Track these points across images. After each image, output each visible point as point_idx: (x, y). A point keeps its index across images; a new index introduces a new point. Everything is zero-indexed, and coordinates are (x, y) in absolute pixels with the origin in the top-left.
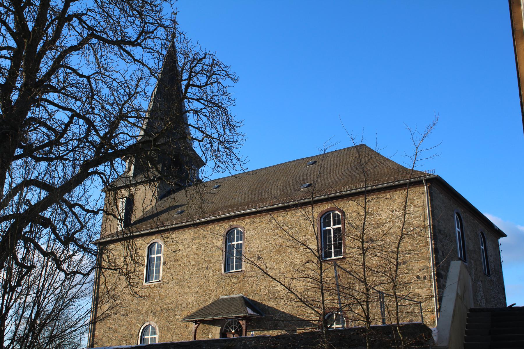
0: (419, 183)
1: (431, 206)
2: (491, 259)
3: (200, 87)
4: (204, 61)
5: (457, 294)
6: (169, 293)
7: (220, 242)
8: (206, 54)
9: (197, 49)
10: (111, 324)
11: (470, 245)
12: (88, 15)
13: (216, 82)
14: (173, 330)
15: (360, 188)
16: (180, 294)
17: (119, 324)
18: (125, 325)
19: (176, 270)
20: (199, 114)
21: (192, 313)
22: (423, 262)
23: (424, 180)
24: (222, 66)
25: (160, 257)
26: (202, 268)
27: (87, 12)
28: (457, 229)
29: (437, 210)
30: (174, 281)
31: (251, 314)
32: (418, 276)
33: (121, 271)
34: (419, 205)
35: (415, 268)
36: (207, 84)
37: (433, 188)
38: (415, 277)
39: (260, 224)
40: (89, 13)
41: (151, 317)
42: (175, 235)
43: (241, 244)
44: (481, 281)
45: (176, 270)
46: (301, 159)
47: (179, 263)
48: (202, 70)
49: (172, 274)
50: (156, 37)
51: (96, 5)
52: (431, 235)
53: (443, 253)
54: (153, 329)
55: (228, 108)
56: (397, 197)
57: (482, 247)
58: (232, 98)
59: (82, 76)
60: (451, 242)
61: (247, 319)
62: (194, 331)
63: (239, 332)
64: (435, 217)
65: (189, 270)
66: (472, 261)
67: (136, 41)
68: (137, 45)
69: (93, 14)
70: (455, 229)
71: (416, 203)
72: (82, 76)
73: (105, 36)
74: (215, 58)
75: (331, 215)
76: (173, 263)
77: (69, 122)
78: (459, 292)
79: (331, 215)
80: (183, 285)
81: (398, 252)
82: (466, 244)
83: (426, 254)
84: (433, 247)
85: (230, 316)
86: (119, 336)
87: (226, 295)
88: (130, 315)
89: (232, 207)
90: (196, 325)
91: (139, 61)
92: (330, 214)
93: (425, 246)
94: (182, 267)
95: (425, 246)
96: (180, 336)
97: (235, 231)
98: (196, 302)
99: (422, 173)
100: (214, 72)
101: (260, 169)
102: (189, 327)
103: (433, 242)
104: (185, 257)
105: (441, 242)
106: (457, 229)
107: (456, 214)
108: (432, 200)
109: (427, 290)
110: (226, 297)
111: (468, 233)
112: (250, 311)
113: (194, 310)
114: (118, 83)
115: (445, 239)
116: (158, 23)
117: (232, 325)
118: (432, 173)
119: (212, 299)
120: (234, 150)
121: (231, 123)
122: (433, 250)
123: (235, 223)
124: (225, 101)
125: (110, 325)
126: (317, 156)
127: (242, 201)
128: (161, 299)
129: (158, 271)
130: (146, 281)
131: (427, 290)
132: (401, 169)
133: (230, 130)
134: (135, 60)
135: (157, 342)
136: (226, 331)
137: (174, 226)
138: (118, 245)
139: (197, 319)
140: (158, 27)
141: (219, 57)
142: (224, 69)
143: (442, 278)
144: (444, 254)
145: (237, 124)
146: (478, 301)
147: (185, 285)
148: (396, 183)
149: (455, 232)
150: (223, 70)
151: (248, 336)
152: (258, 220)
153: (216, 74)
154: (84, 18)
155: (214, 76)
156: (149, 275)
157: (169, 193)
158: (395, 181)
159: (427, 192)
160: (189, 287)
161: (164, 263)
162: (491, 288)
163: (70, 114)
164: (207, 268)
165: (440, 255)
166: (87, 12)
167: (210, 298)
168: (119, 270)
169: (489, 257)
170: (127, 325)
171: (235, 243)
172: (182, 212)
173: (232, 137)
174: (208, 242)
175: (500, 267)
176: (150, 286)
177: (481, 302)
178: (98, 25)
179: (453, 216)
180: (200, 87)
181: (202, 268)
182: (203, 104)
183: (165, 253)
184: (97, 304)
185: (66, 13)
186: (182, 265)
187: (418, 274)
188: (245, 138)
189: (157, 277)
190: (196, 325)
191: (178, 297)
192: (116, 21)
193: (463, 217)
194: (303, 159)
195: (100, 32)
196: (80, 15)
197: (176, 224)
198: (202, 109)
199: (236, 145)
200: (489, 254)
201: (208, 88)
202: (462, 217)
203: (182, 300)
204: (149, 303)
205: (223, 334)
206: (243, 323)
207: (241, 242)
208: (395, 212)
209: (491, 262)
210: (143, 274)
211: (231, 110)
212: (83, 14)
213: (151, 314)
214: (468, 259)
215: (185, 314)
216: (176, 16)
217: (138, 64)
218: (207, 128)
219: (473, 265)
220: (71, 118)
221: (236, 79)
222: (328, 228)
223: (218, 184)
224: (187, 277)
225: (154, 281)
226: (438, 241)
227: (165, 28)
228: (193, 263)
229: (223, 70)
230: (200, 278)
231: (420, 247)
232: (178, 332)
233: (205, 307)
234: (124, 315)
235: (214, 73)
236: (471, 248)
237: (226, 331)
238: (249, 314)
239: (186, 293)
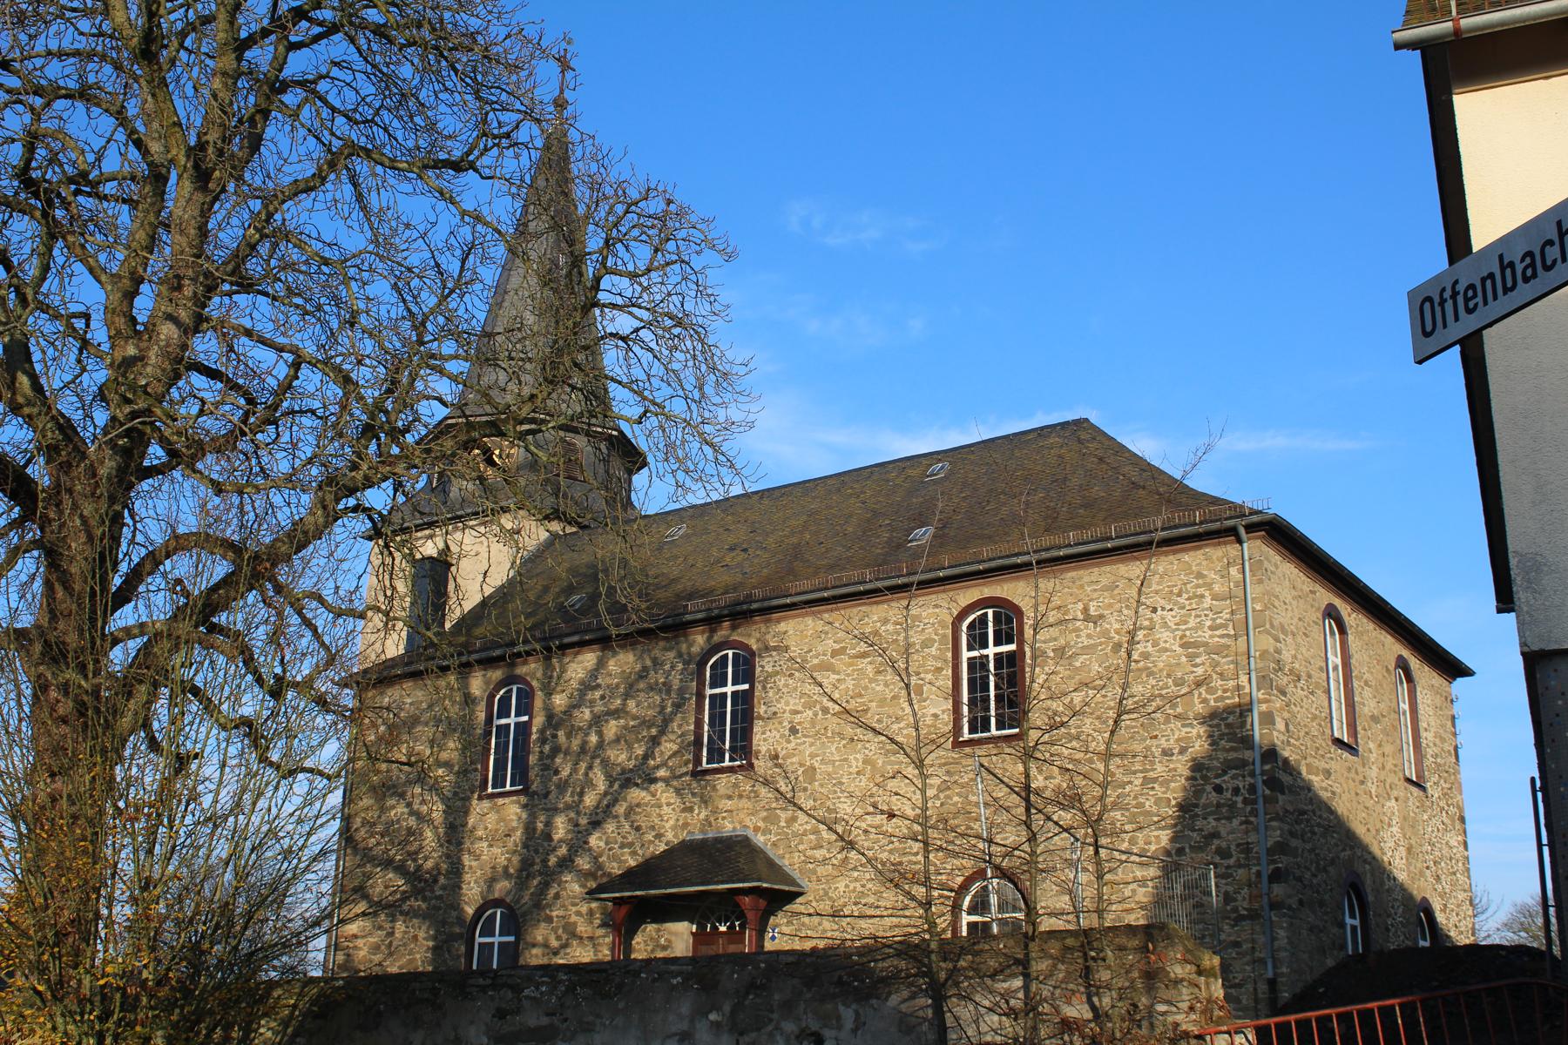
3: (633, 276)
12: (332, 78)
13: (675, 262)
38: (1209, 788)
40: (335, 72)
44: (1397, 800)
69: (346, 76)
105: (1284, 693)
109: (1241, 824)
124: (698, 309)
131: (1241, 824)
143: (1283, 793)
154: (323, 86)
162: (1425, 817)
165: (1279, 731)
171: (497, 939)
187: (1217, 781)
208: (1159, 612)
211: (719, 333)
221: (729, 250)
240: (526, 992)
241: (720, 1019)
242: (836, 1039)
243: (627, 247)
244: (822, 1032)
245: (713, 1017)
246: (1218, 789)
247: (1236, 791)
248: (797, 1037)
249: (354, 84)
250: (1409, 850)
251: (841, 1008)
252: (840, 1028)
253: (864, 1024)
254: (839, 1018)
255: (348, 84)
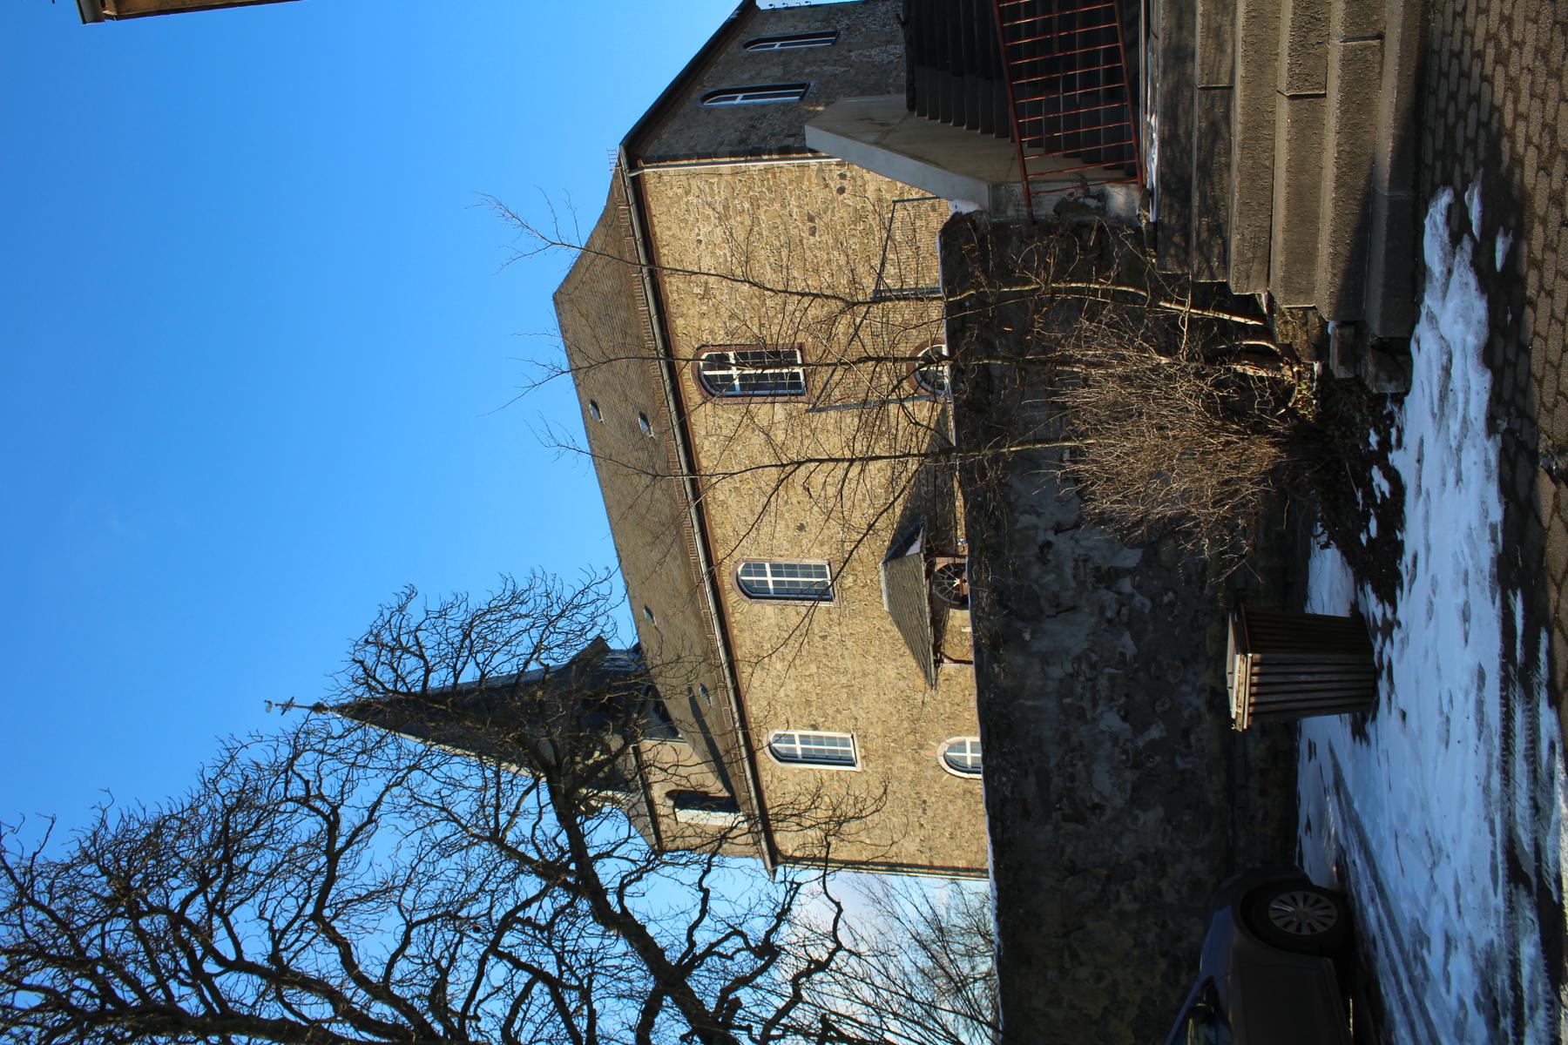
0: (638, 185)
1: (688, 159)
2: (802, 28)
4: (369, 663)
5: (876, 144)
6: (879, 718)
7: (768, 611)
8: (354, 660)
9: (345, 680)
10: (942, 835)
11: (773, 74)
12: (273, 916)
14: (956, 707)
15: (649, 310)
16: (879, 695)
17: (943, 819)
18: (945, 807)
19: (829, 702)
20: (488, 669)
21: (918, 669)
22: (809, 180)
23: (630, 172)
24: (380, 622)
25: (800, 736)
26: (824, 648)
27: (266, 919)
28: (737, 101)
29: (695, 146)
30: (852, 707)
31: (921, 547)
32: (838, 191)
33: (831, 833)
34: (685, 184)
35: (821, 195)
36: (422, 657)
37: (648, 154)
38: (840, 198)
39: (728, 526)
40: (268, 915)
41: (927, 753)
42: (754, 709)
43: (771, 566)
44: (850, 51)
45: (829, 702)
46: (587, 432)
47: (814, 697)
48: (391, 665)
49: (838, 711)
50: (318, 772)
51: (250, 901)
52: (751, 161)
53: (790, 136)
54: (952, 748)
55: (473, 607)
56: (668, 233)
57: (776, 47)
58: (451, 599)
59: (406, 941)
60: (765, 116)
61: (930, 554)
62: (957, 665)
63: (958, 571)
64: (710, 151)
65: (829, 677)
66: (807, 70)
67: (326, 818)
68: (337, 816)
69: (271, 905)
70: (738, 106)
71: (680, 191)
72: (406, 941)
73: (320, 879)
74: (363, 639)
75: (707, 373)
76: (814, 709)
77: (509, 961)
78: (873, 138)
79: (707, 373)
80: (860, 689)
81: (786, 291)
82: (769, 83)
83: (791, 171)
84: (777, 157)
85: (926, 591)
86: (967, 817)
87: (881, 597)
88: (925, 797)
89: (695, 589)
90: (946, 660)
91: (372, 813)
92: (705, 376)
93: (774, 174)
94: (822, 690)
95: (774, 174)
96: (967, 693)
97: (743, 578)
98: (895, 660)
99: (615, 177)
100: (394, 639)
101: (610, 521)
102: (949, 675)
103: (766, 157)
104: (802, 685)
105: (764, 139)
106: (737, 101)
107: (705, 104)
108: (675, 158)
110: (885, 598)
111: (746, 76)
112: (915, 548)
113: (912, 663)
114: (420, 860)
115: (759, 129)
116: (286, 771)
117: (943, 583)
118: (616, 157)
119: (889, 627)
120: (568, 596)
121: (506, 602)
122: (782, 156)
123: (727, 582)
124: (458, 616)
125: (945, 836)
126: (580, 399)
127: (679, 562)
128: (890, 732)
129: (832, 741)
130: (853, 765)
132: (608, 220)
133: (521, 603)
134: (370, 821)
135: (977, 739)
136: (956, 598)
137: (734, 709)
138: (778, 837)
139: (932, 658)
140: (293, 772)
141: (361, 631)
142: (387, 618)
144: (792, 133)
145: (510, 586)
146: (892, 61)
147: (859, 683)
148: (638, 235)
149: (745, 108)
150: (389, 621)
151: (966, 552)
152: (719, 531)
153: (399, 635)
155: (404, 639)
156: (840, 759)
157: (665, 716)
158: (634, 235)
159: (658, 167)
160: (864, 675)
161: (815, 727)
162: (864, 30)
163: (492, 960)
164: (824, 637)
166: (266, 919)
167: (887, 631)
168: (829, 839)
169: (799, 31)
170: (946, 802)
171: (770, 579)
172: (705, 690)
173: (538, 599)
174: (767, 636)
175: (820, 8)
176: (863, 757)
177: (894, 54)
178: (295, 894)
179: (709, 111)
180: (428, 671)
181: (824, 648)
182: (465, 664)
183: (791, 725)
184: (902, 865)
185: (269, 970)
186: (818, 691)
188: (539, 574)
189: (844, 742)
190: (946, 660)
191: (887, 698)
192: (285, 856)
193: (713, 86)
194: (586, 428)
195: (310, 889)
196: (274, 936)
197: (730, 703)
198: (477, 664)
199: (554, 593)
200: (792, 31)
201: (427, 654)
202: (711, 90)
203: (893, 689)
204: (900, 758)
205: (962, 603)
206: (941, 562)
207: (767, 565)
209: (808, 27)
210: (838, 772)
211: (479, 601)
212: (271, 928)
213: (922, 752)
214: (802, 80)
215: (920, 682)
216: (274, 703)
217: (377, 814)
218: (518, 653)
219: (815, 69)
220: (501, 956)
222: (737, 382)
223: (644, 613)
224: (844, 681)
225: (852, 749)
226: (763, 145)
227: (296, 756)
228: (813, 668)
229: (389, 621)
230: (846, 652)
231: (776, 184)
232: (960, 696)
233: (907, 642)
234: (924, 810)
235: (397, 640)
236: (777, 72)
237: (956, 598)
238: (921, 551)
239: (878, 680)
240: (1008, 793)
241: (1029, 630)
242: (1045, 530)
243: (410, 673)
244: (1040, 543)
245: (1027, 637)
246: (841, 190)
247: (843, 176)
248: (1045, 564)
249: (279, 899)
250: (889, 42)
251: (1019, 526)
252: (1035, 527)
253: (1032, 506)
254: (1027, 528)
255: (279, 903)
